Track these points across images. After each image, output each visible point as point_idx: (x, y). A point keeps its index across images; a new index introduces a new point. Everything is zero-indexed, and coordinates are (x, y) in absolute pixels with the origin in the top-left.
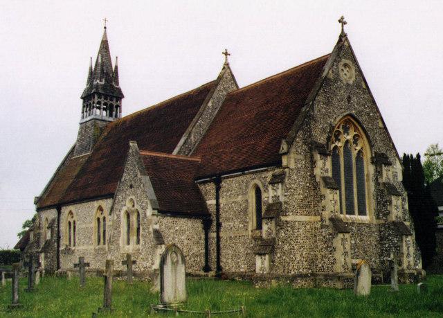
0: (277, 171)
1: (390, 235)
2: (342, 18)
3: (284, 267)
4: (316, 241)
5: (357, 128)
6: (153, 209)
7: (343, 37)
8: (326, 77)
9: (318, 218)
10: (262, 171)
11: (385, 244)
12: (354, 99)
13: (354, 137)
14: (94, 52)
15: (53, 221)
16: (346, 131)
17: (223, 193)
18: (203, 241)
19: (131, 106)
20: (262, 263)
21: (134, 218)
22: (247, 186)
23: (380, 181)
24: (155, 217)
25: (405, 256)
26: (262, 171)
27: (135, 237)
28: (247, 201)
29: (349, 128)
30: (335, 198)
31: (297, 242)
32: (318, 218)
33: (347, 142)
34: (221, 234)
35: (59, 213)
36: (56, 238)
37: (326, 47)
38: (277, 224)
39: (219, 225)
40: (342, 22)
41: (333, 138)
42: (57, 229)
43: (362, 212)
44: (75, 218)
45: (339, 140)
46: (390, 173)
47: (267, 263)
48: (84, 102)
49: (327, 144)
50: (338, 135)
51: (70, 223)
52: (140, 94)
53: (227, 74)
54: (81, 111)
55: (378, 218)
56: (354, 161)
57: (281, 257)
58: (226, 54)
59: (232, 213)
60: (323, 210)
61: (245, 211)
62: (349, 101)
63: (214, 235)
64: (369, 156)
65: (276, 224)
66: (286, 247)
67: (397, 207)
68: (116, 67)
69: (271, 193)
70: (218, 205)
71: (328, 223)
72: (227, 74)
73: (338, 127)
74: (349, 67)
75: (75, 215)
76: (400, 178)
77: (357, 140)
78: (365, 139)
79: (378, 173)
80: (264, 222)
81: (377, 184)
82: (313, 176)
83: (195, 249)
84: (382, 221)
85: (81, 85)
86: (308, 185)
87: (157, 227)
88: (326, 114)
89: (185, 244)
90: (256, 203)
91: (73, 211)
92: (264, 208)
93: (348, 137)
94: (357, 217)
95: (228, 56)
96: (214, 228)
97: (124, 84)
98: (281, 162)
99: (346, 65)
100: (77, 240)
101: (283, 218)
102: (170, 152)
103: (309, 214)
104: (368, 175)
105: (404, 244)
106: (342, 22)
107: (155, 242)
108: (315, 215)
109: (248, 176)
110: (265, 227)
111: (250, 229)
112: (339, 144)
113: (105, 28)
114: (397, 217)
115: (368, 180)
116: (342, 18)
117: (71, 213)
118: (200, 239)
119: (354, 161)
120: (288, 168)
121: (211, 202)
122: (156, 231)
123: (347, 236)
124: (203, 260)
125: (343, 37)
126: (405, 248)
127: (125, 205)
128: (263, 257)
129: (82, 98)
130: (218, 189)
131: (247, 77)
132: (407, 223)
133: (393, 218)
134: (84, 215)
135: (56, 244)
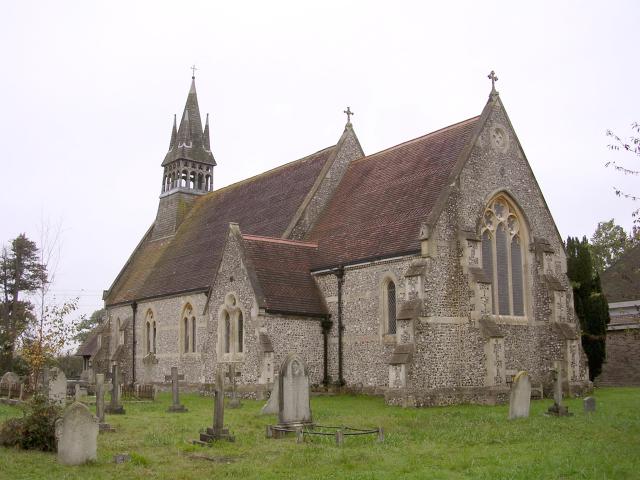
0: (416, 261)
2: (493, 73)
6: (260, 308)
7: (494, 96)
10: (396, 261)
12: (509, 172)
14: (179, 108)
15: (127, 322)
16: (500, 211)
21: (235, 320)
22: (377, 280)
26: (396, 261)
27: (237, 344)
28: (377, 298)
32: (466, 320)
33: (501, 224)
34: (344, 340)
35: (135, 311)
37: (472, 108)
39: (341, 328)
40: (492, 77)
41: (484, 220)
43: (519, 312)
44: (155, 319)
45: (491, 223)
47: (402, 376)
48: (165, 171)
53: (349, 138)
56: (509, 248)
58: (348, 113)
61: (375, 310)
63: (335, 340)
64: (527, 242)
66: (426, 356)
67: (560, 306)
68: (207, 127)
69: (408, 288)
71: (477, 325)
72: (349, 138)
74: (502, 133)
75: (155, 314)
76: (564, 269)
79: (539, 263)
80: (399, 324)
81: (537, 277)
82: (459, 267)
84: (542, 323)
85: (163, 149)
87: (264, 330)
88: (477, 192)
91: (153, 310)
92: (399, 307)
93: (502, 219)
94: (512, 318)
97: (216, 148)
99: (498, 131)
101: (422, 320)
105: (569, 350)
106: (492, 77)
107: (262, 349)
110: (400, 331)
111: (381, 333)
113: (193, 78)
115: (526, 272)
116: (493, 73)
117: (150, 311)
119: (509, 248)
121: (331, 300)
122: (264, 337)
123: (501, 341)
125: (494, 96)
126: (570, 355)
127: (223, 303)
129: (163, 166)
131: (373, 144)
132: (572, 325)
133: (555, 319)
134: (167, 315)
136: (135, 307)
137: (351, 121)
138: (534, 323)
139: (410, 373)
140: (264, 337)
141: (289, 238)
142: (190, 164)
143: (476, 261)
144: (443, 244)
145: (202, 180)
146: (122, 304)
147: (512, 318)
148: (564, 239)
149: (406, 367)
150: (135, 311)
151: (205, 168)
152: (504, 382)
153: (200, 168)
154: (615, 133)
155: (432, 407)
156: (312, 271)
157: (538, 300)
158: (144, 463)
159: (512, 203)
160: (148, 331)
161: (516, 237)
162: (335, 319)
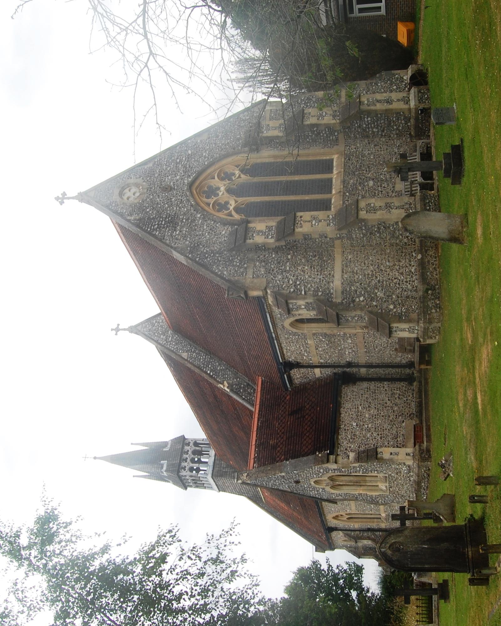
2: (57, 199)
3: (407, 297)
5: (209, 174)
6: (328, 461)
9: (338, 242)
11: (373, 132)
13: (222, 179)
14: (128, 473)
15: (346, 535)
16: (213, 192)
17: (305, 359)
18: (372, 385)
20: (404, 330)
23: (284, 140)
25: (391, 107)
28: (314, 334)
29: (210, 187)
30: (309, 218)
31: (372, 275)
32: (338, 242)
33: (229, 191)
35: (336, 529)
38: (347, 308)
39: (349, 365)
40: (62, 199)
42: (358, 532)
43: (327, 166)
45: (227, 203)
46: (272, 124)
48: (191, 486)
50: (219, 204)
51: (349, 518)
52: (176, 418)
53: (146, 329)
54: (204, 490)
55: (336, 142)
57: (393, 303)
58: (117, 330)
59: (332, 350)
60: (326, 237)
61: (325, 335)
62: (171, 189)
65: (347, 310)
70: (321, 366)
72: (146, 329)
75: (337, 514)
77: (226, 173)
83: (383, 397)
84: (341, 136)
85: (170, 489)
86: (289, 257)
87: (352, 455)
89: (376, 412)
91: (334, 515)
94: (336, 176)
95: (120, 327)
96: (355, 370)
97: (167, 435)
98: (258, 298)
100: (370, 512)
102: (251, 413)
104: (275, 157)
105: (373, 108)
108: (333, 246)
109: (279, 332)
112: (232, 205)
113: (95, 458)
116: (57, 199)
117: (336, 518)
122: (359, 459)
124: (398, 385)
126: (379, 106)
128: (395, 329)
129: (186, 489)
130: (298, 365)
131: (146, 304)
133: (330, 230)
135: (377, 533)
136: (331, 529)
137: (127, 327)
138: (341, 147)
139: (400, 318)
140: (359, 459)
141: (253, 405)
142: (184, 464)
143: (269, 228)
146: (329, 539)
147: (336, 176)
149: (394, 322)
150: (336, 529)
152: (412, 200)
153: (187, 453)
155: (440, 288)
157: (314, 141)
160: (355, 518)
162: (340, 370)
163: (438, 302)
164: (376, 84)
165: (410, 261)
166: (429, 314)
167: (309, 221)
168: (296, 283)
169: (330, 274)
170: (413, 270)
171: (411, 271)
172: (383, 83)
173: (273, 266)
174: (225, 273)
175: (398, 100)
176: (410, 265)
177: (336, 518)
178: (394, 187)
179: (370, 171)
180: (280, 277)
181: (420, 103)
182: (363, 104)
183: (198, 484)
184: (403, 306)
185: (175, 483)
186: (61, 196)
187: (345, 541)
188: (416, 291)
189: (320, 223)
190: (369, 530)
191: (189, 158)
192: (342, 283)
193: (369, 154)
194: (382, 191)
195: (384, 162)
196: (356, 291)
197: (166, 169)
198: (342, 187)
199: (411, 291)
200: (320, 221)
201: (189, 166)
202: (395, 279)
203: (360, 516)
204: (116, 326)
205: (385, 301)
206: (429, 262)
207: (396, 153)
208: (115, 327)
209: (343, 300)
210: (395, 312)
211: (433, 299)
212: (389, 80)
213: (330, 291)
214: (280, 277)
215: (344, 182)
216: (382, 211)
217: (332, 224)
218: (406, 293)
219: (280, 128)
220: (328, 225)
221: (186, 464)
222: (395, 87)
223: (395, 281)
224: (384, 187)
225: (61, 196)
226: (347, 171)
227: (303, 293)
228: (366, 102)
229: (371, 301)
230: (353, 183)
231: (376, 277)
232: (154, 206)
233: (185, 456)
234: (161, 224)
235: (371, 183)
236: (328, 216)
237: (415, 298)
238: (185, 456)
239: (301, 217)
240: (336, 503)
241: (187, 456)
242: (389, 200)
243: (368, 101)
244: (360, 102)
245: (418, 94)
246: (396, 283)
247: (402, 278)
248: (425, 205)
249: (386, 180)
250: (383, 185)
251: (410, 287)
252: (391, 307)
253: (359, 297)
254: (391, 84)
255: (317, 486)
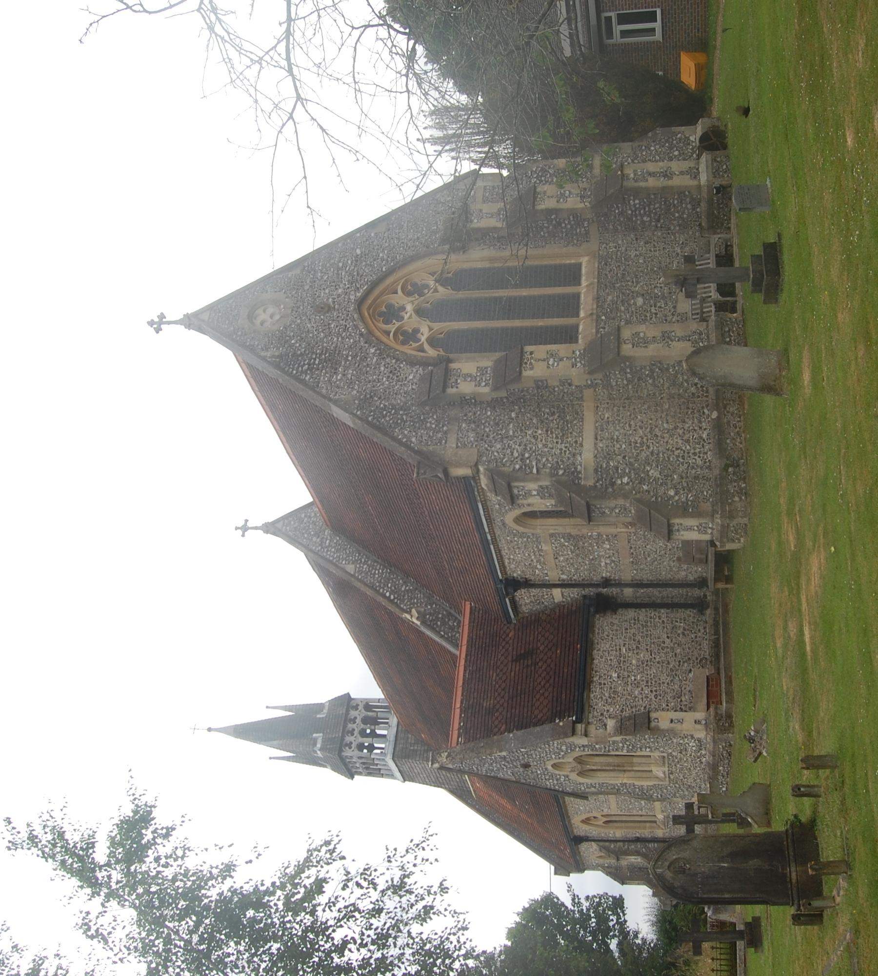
1: (621, 213)
2: (151, 323)
3: (696, 478)
4: (640, 398)
6: (574, 733)
8: (277, 366)
9: (588, 393)
11: (643, 222)
13: (408, 294)
14: (262, 753)
15: (601, 848)
18: (642, 614)
19: (359, 680)
20: (690, 529)
24: (592, 728)
25: (670, 183)
28: (552, 535)
29: (390, 307)
30: (543, 355)
31: (642, 443)
32: (588, 393)
36: (639, 845)
40: (158, 324)
42: (621, 844)
43: (572, 275)
44: (598, 815)
45: (416, 331)
48: (360, 774)
49: (424, 363)
50: (404, 333)
52: (339, 668)
53: (287, 528)
57: (675, 487)
58: (245, 528)
59: (580, 560)
60: (570, 385)
61: (568, 537)
62: (330, 309)
70: (563, 585)
72: (287, 528)
73: (387, 333)
77: (414, 285)
78: (411, 267)
85: (327, 777)
87: (611, 723)
90: (557, 517)
91: (584, 817)
93: (409, 308)
94: (585, 290)
95: (249, 525)
96: (614, 591)
97: (321, 692)
98: (465, 478)
100: (640, 813)
102: (454, 659)
103: (579, 416)
104: (492, 260)
105: (642, 184)
106: (158, 324)
109: (498, 532)
113: (210, 730)
114: (582, 197)
116: (151, 323)
117: (586, 821)
118: (636, 620)
120: (476, 465)
122: (621, 729)
123: (626, 334)
124: (681, 613)
126: (652, 182)
128: (676, 527)
129: (352, 777)
130: (527, 584)
131: (293, 492)
133: (577, 374)
135: (650, 845)
136: (579, 840)
139: (684, 510)
140: (621, 729)
141: (456, 645)
142: (348, 739)
143: (482, 370)
144: (452, 442)
145: (371, 714)
146: (575, 854)
147: (585, 290)
148: (447, 168)
151: (353, 713)
153: (354, 721)
154: (214, 865)
156: (509, 621)
158: (862, 16)
159: (376, 292)
161: (442, 281)
162: (591, 591)
163: (743, 485)
164: (648, 148)
165: (700, 422)
166: (730, 504)
167: (544, 360)
168: (523, 455)
169: (576, 442)
170: (704, 436)
171: (701, 438)
172: (657, 147)
173: (487, 430)
174: (414, 440)
175: (682, 173)
176: (701, 428)
177: (586, 821)
178: (675, 307)
179: (637, 283)
180: (498, 446)
181: (715, 177)
182: (628, 179)
183: (372, 769)
184: (690, 491)
185: (335, 769)
186: (156, 320)
187: (600, 857)
188: (709, 468)
189: (561, 363)
190: (638, 840)
191: (357, 261)
192: (595, 456)
193: (636, 256)
194: (656, 314)
195: (660, 268)
196: (617, 468)
197: (322, 278)
198: (595, 306)
199: (701, 468)
200: (561, 360)
201: (358, 274)
202: (677, 449)
203: (624, 818)
204: (243, 523)
205: (662, 484)
206: (729, 422)
207: (678, 254)
208: (241, 523)
209: (597, 482)
210: (677, 501)
211: (735, 481)
212: (667, 141)
213: (576, 468)
214: (498, 446)
215: (597, 299)
216: (656, 345)
217: (579, 364)
218: (693, 471)
219: (499, 214)
220: (574, 365)
221: (352, 739)
222: (676, 153)
223: (676, 453)
224: (660, 307)
225: (156, 320)
226: (603, 283)
227: (535, 471)
228: (632, 175)
229: (640, 483)
230: (612, 301)
231: (648, 447)
232: (303, 336)
233: (350, 726)
234: (314, 363)
235: (640, 301)
236: (574, 352)
237: (708, 479)
238: (350, 726)
239: (531, 353)
240: (586, 798)
241: (354, 726)
242: (667, 327)
243: (635, 175)
244: (623, 175)
245: (712, 164)
246: (678, 456)
247: (688, 447)
248: (722, 335)
249: (664, 297)
250: (659, 304)
251: (699, 462)
252: (672, 493)
253: (621, 477)
254: (671, 148)
255: (557, 772)
